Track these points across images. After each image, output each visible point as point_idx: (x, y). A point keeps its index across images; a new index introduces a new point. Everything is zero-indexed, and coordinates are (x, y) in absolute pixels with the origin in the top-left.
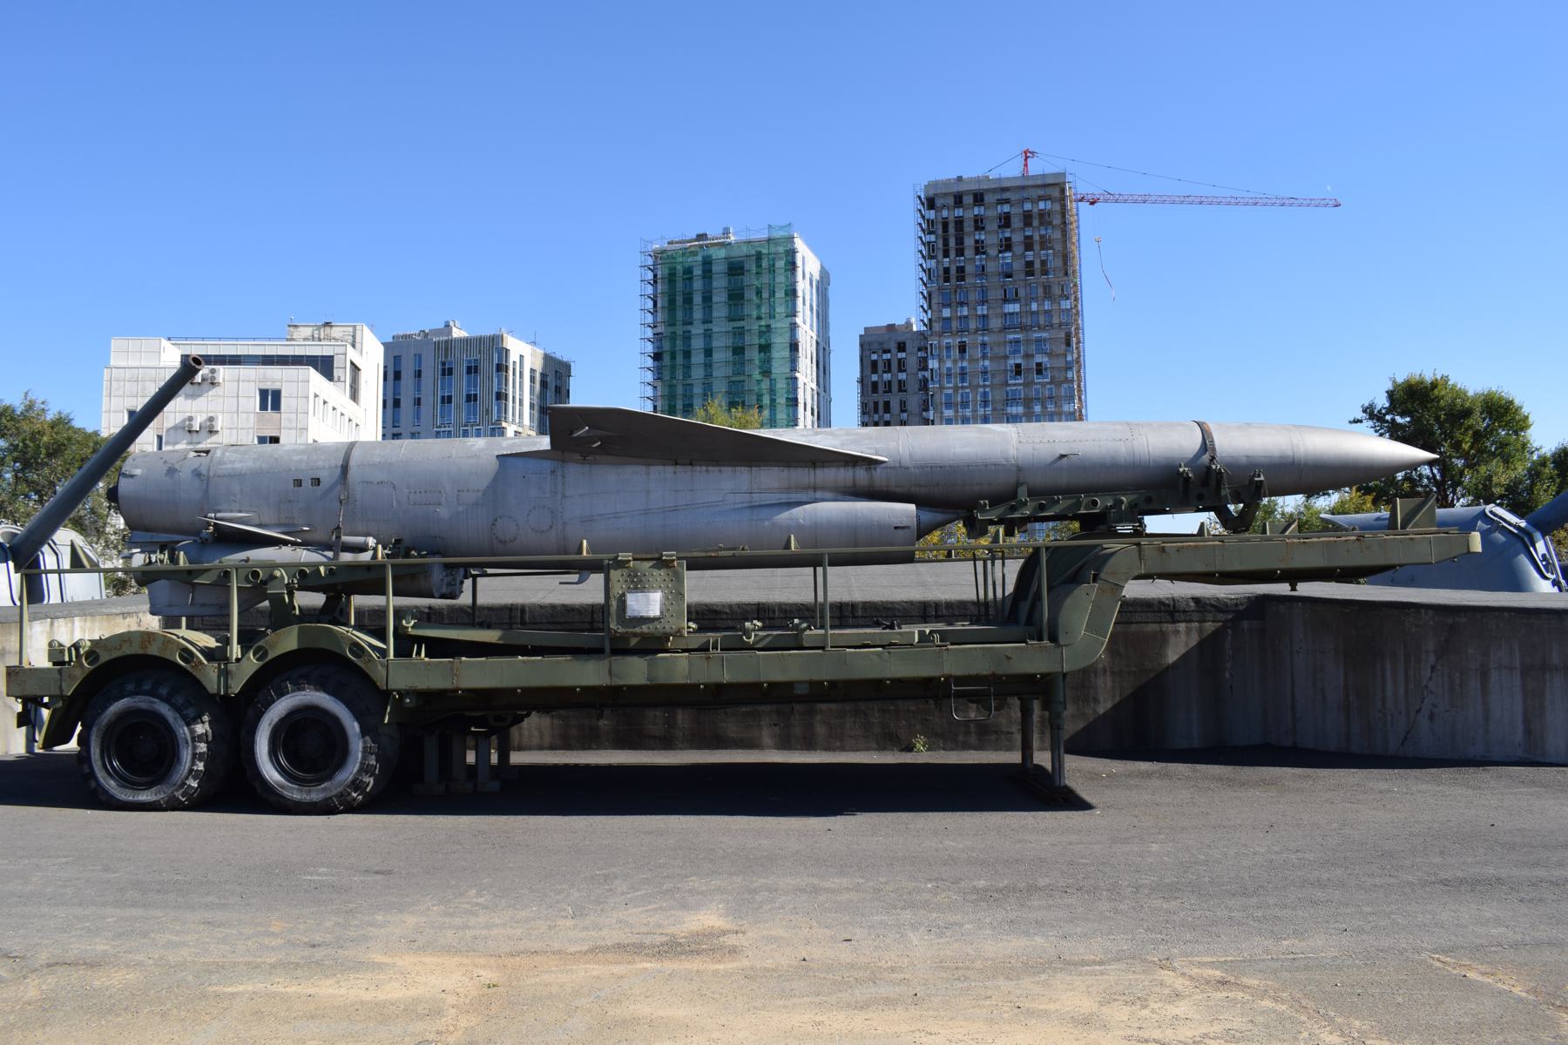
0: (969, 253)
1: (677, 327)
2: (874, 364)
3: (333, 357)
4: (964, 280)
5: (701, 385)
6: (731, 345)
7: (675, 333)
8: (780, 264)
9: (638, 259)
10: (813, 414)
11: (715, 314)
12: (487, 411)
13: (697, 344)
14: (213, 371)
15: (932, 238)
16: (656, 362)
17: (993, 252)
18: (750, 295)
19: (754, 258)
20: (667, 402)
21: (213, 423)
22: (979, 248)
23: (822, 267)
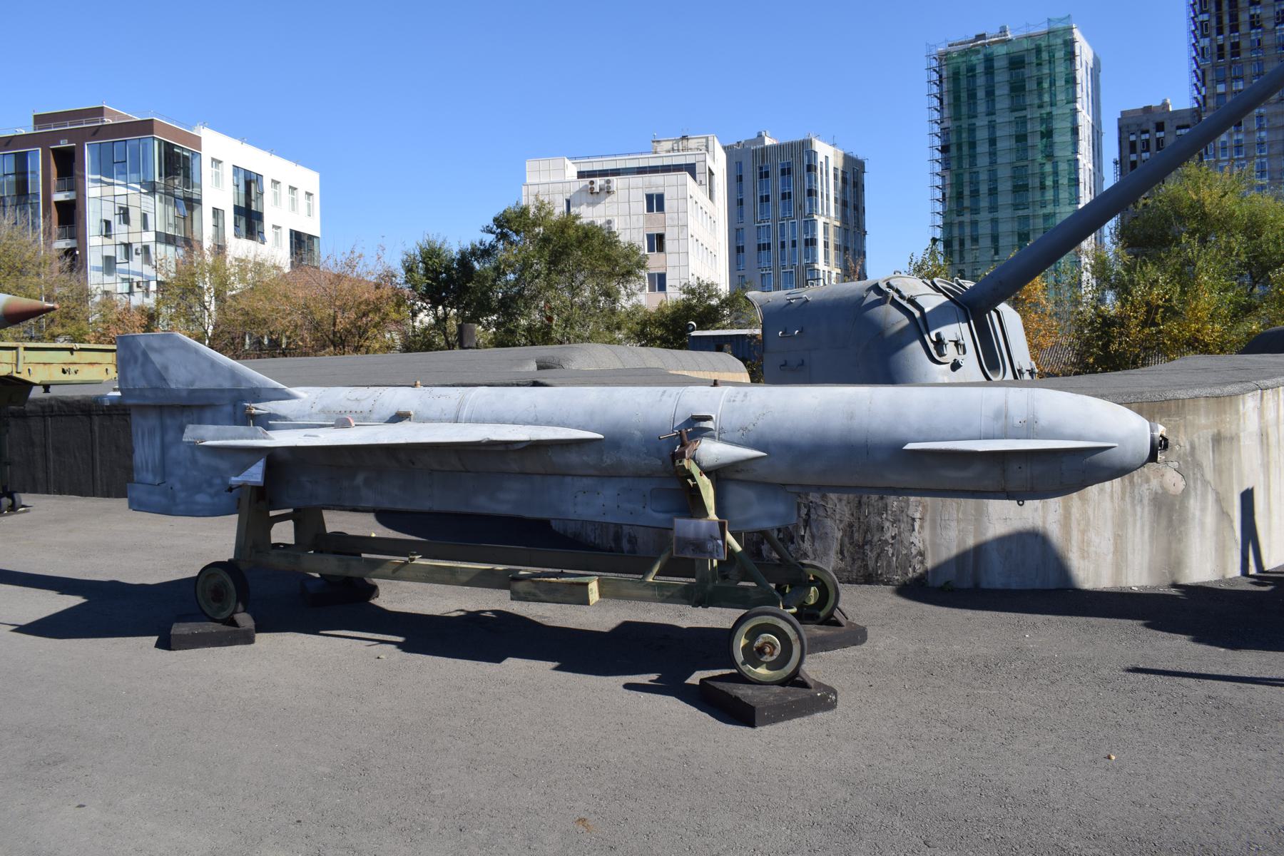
0: (1244, 28)
1: (963, 121)
2: (1133, 147)
3: (695, 164)
4: (1238, 55)
5: (986, 172)
6: (1014, 133)
7: (961, 126)
8: (1060, 54)
9: (924, 63)
10: (1090, 193)
11: (998, 106)
12: (800, 206)
13: (982, 135)
14: (608, 182)
15: (1206, 17)
16: (944, 154)
17: (1269, 25)
18: (1031, 85)
19: (1034, 51)
20: (955, 189)
21: (611, 225)
22: (1255, 23)
23: (1095, 55)
